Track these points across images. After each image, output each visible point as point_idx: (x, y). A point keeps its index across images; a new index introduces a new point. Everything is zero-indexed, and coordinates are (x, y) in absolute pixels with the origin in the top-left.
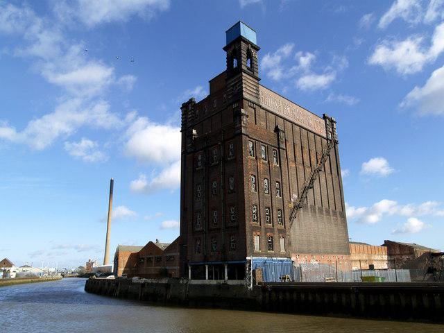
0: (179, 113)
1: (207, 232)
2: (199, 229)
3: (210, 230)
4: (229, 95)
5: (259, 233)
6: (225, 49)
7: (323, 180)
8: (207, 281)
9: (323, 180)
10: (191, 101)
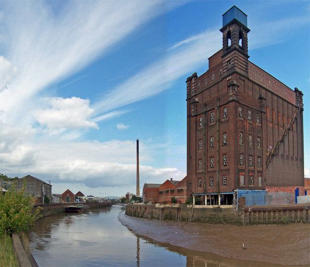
0: (185, 85)
1: (206, 173)
2: (200, 171)
3: (208, 172)
4: (224, 70)
5: (243, 174)
6: (222, 30)
7: (291, 137)
8: (206, 206)
9: (291, 137)
10: (195, 75)
